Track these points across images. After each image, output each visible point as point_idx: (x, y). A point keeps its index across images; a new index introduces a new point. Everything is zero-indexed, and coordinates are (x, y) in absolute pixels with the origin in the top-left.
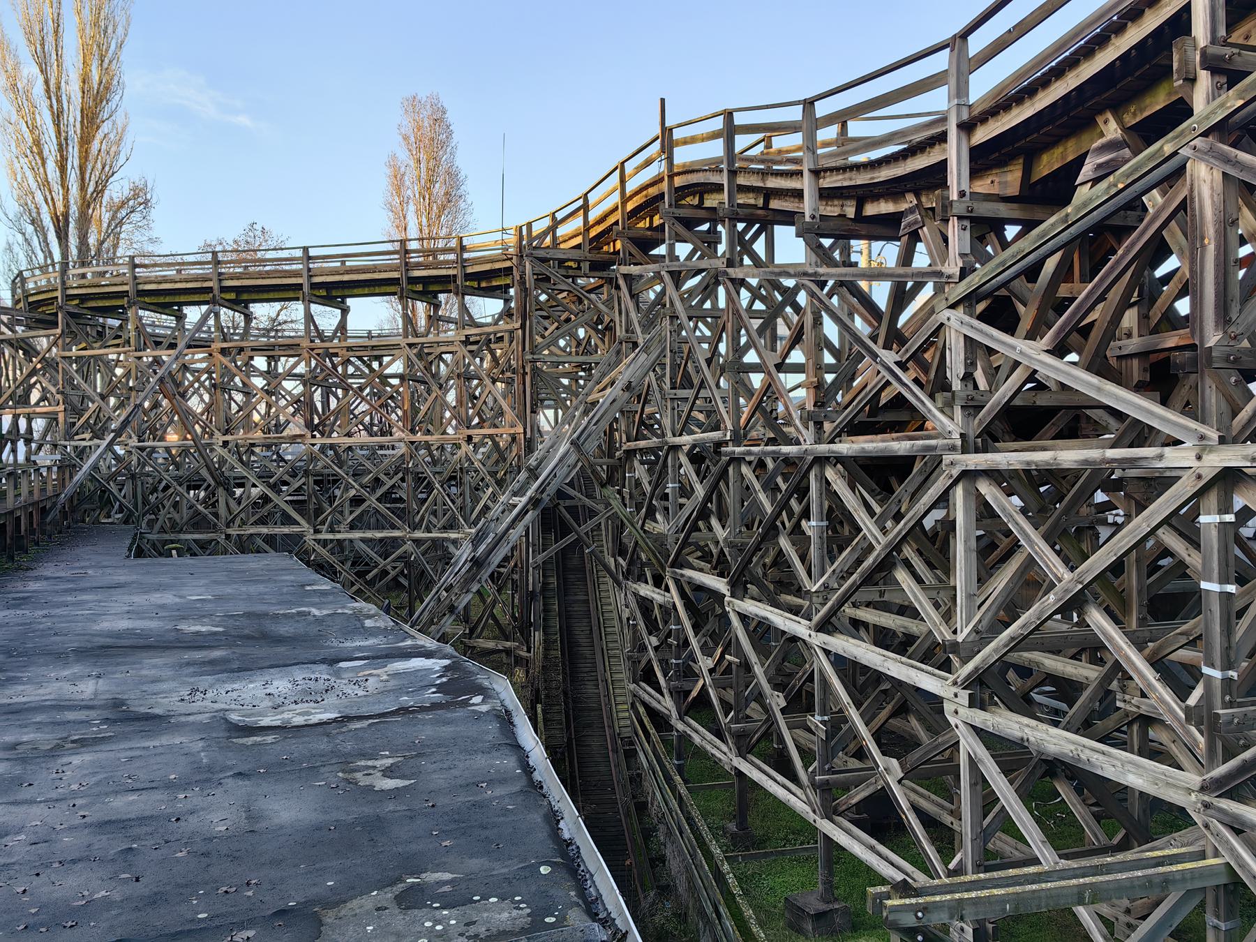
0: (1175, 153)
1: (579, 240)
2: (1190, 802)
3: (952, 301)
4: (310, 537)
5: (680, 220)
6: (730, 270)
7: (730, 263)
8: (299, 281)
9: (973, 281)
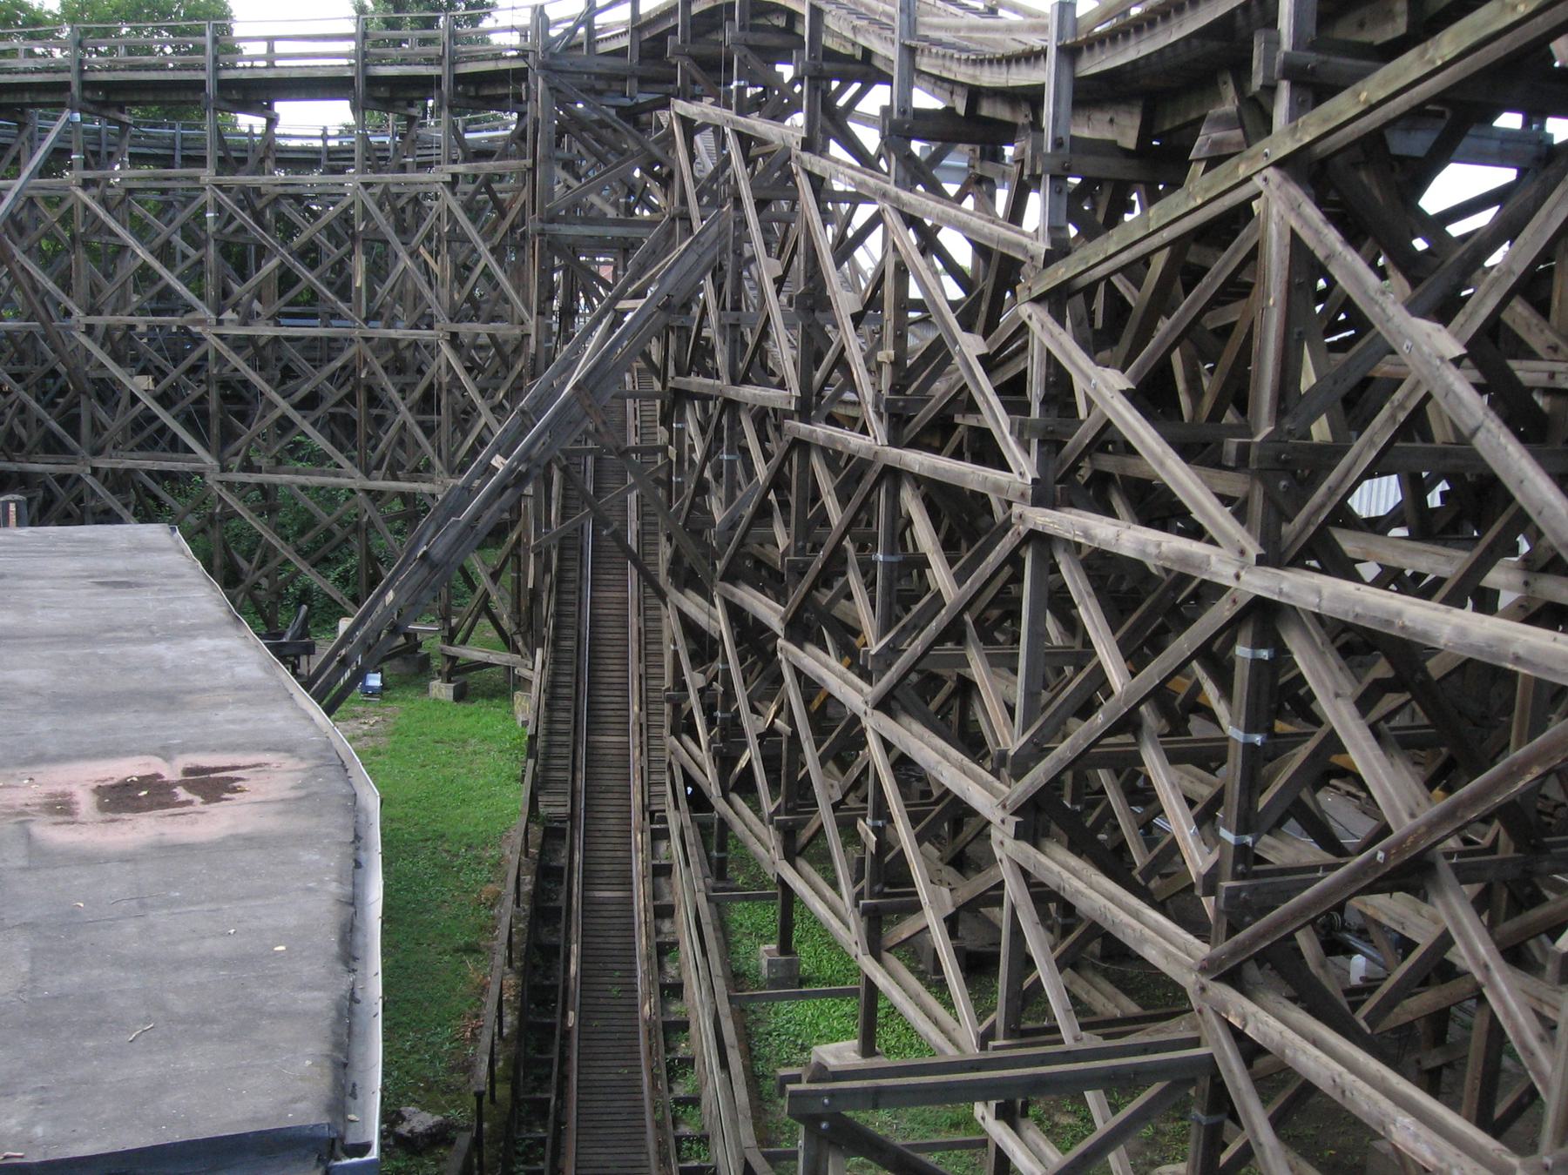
0: (1248, 179)
1: (625, 42)
2: (1189, 980)
3: (1035, 294)
4: (212, 479)
5: (756, 49)
6: (806, 156)
7: (807, 145)
8: (201, 76)
9: (1061, 272)
